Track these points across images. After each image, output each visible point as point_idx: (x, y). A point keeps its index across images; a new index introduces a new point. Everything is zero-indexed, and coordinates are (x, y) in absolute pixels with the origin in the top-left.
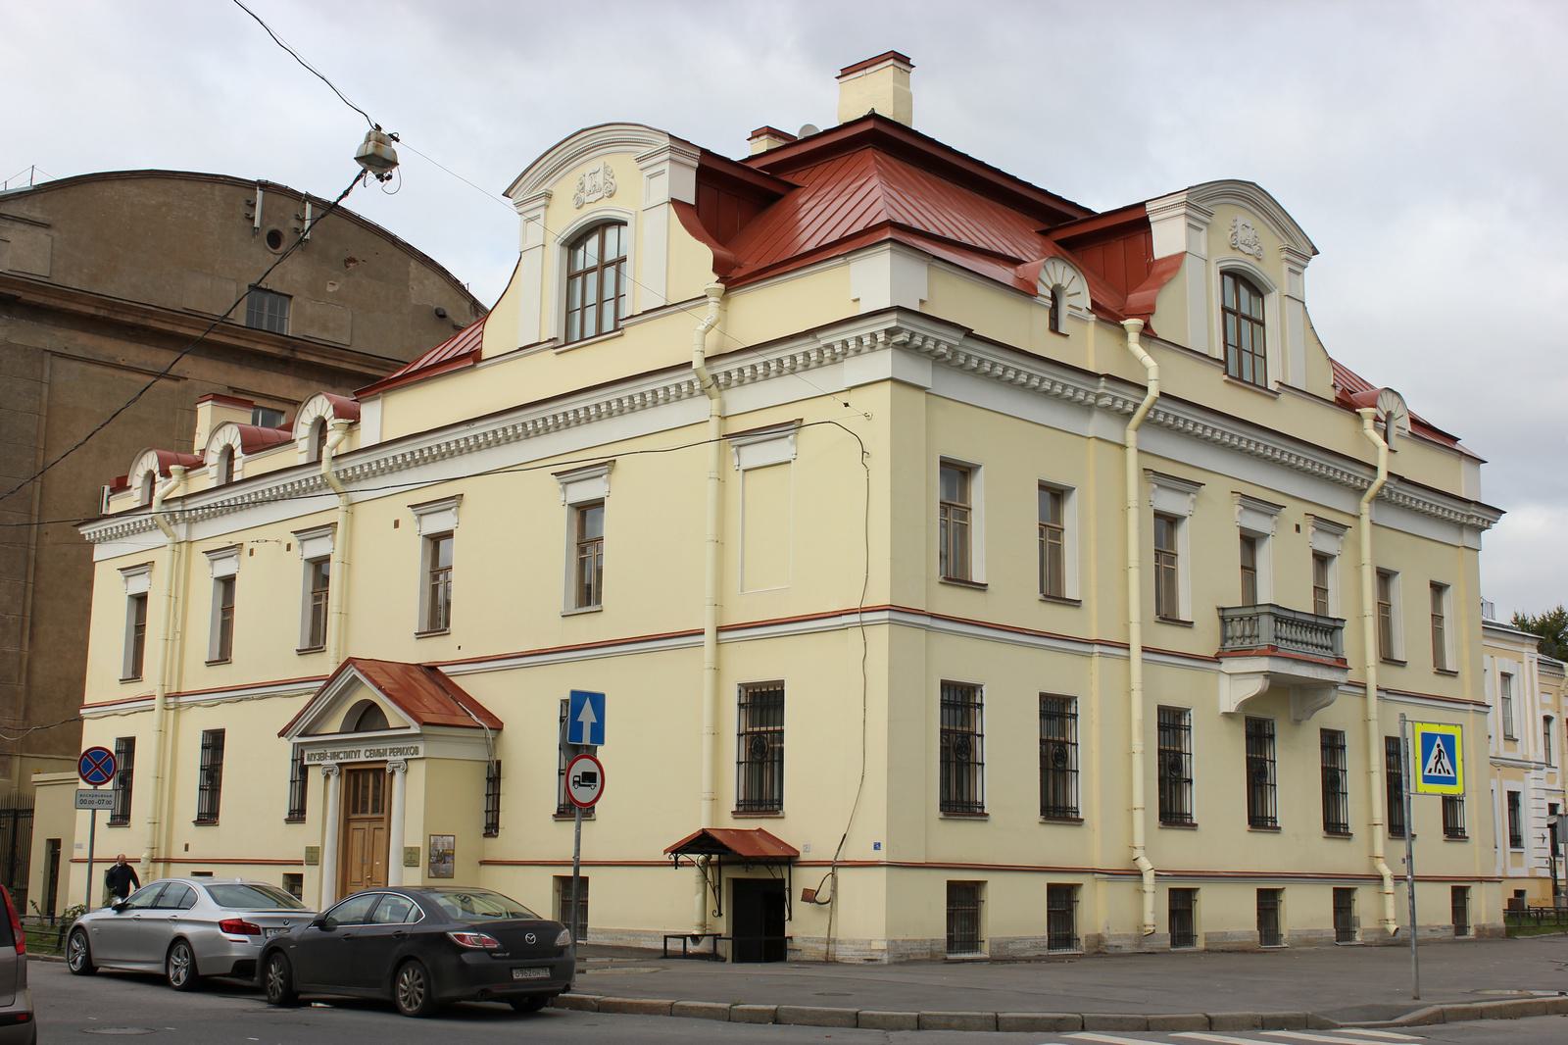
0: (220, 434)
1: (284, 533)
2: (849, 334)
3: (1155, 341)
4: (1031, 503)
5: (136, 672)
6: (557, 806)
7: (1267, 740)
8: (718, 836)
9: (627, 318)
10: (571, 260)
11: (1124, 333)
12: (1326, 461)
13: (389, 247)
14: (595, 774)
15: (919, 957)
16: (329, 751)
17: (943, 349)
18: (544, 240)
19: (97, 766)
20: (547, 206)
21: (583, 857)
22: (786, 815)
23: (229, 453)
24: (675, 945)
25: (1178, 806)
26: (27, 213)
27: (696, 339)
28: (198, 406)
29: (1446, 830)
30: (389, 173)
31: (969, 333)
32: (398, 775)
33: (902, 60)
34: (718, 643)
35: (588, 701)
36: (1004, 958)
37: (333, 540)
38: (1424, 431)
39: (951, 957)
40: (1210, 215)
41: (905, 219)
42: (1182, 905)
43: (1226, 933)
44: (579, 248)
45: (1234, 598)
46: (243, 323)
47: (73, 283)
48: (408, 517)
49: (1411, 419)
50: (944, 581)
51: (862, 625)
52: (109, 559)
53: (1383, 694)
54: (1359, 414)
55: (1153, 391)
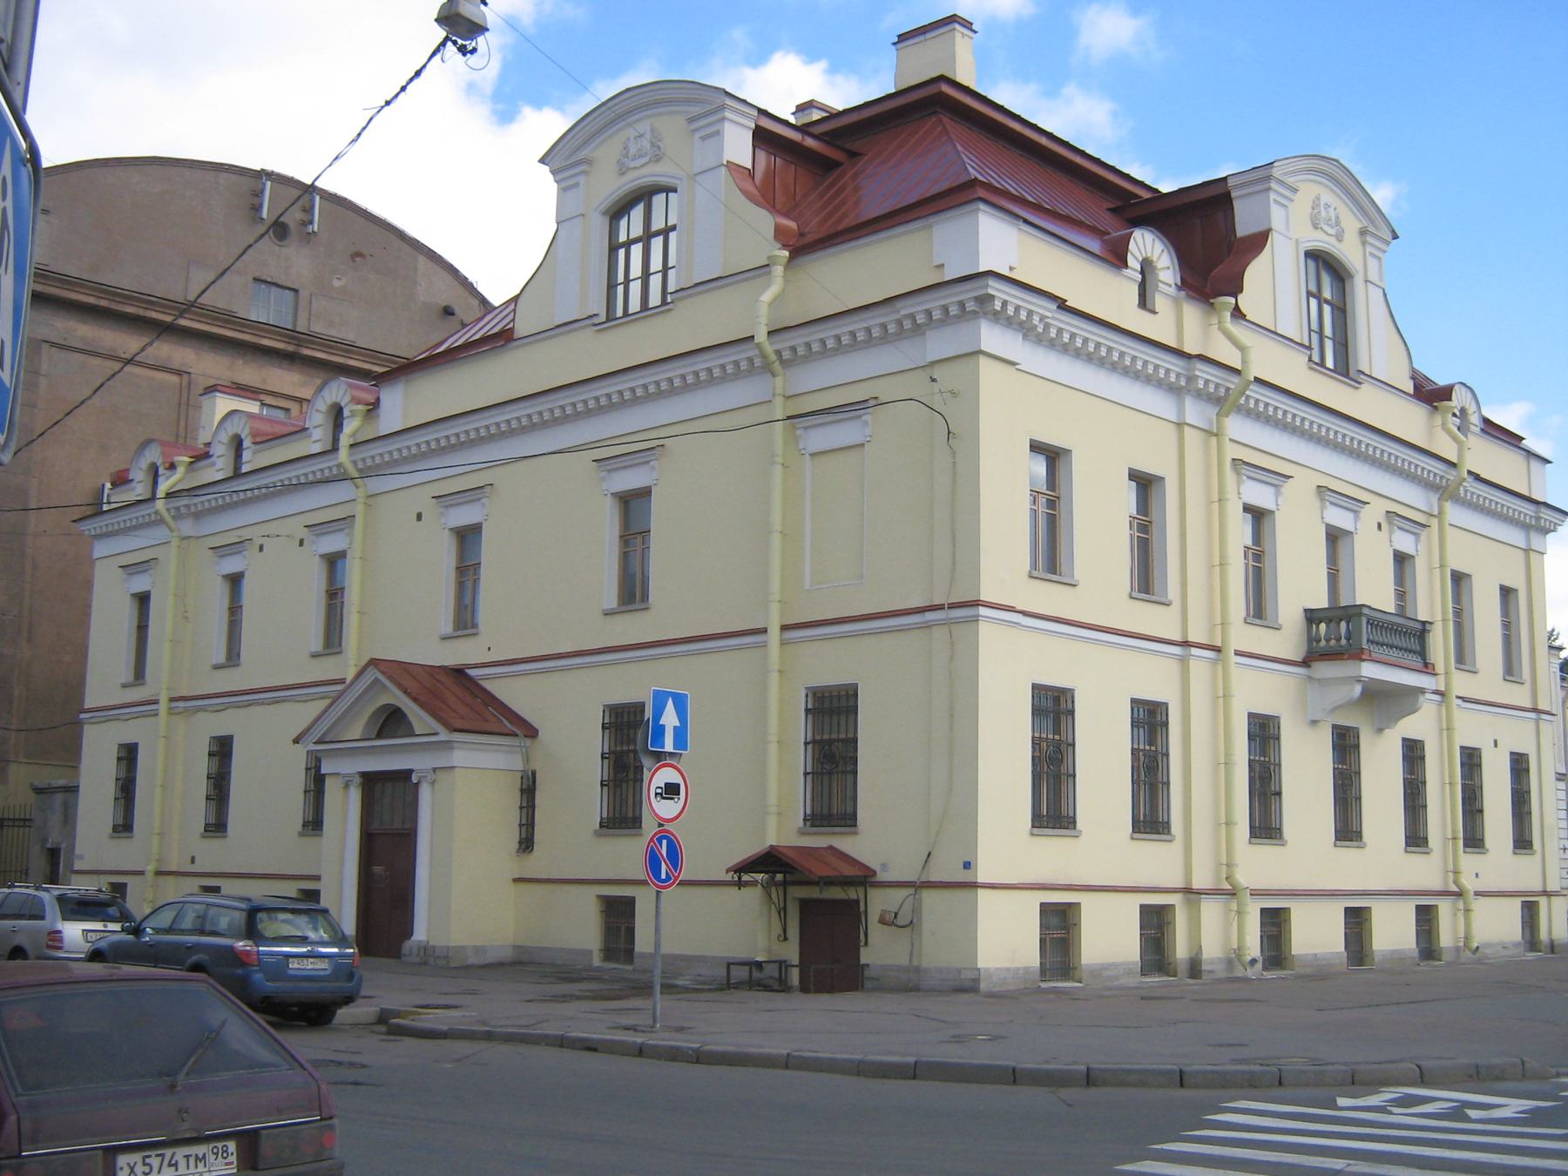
0: (228, 424)
1: (297, 528)
2: (934, 302)
6: (599, 820)
10: (613, 232)
12: (1409, 455)
13: (398, 243)
14: (678, 785)
23: (237, 444)
25: (1165, 815)
30: (474, 44)
31: (1062, 305)
34: (783, 643)
39: (1044, 985)
40: (1295, 190)
44: (623, 216)
45: (1321, 601)
47: (73, 271)
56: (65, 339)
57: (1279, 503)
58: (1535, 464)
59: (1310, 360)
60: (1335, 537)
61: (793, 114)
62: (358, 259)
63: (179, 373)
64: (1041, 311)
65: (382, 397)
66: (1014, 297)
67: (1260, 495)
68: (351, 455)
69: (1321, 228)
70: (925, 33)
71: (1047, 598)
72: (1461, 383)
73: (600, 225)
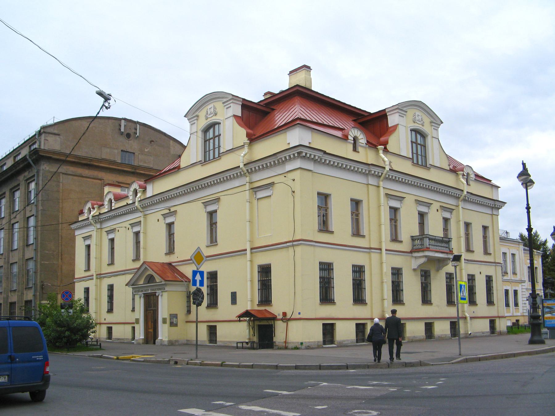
1: (127, 225)
2: (287, 154)
3: (388, 153)
4: (315, 202)
5: (88, 269)
7: (428, 277)
8: (253, 312)
9: (222, 153)
11: (377, 150)
15: (314, 347)
16: (140, 290)
17: (317, 158)
18: (197, 130)
19: (67, 296)
20: (197, 120)
21: (199, 320)
22: (273, 305)
23: (110, 201)
24: (240, 345)
26: (53, 131)
27: (241, 158)
28: (104, 187)
29: (488, 302)
31: (325, 152)
32: (160, 297)
33: (309, 68)
34: (251, 253)
35: (198, 273)
36: (342, 345)
37: (141, 226)
38: (480, 179)
41: (311, 119)
42: (429, 327)
43: (415, 336)
45: (416, 233)
46: (120, 162)
48: (161, 218)
49: (475, 175)
50: (319, 231)
51: (293, 246)
52: (79, 234)
53: (466, 261)
54: (457, 173)
55: (387, 168)
56: (67, 172)
57: (402, 205)
58: (494, 189)
59: (413, 162)
60: (422, 215)
61: (263, 96)
62: (152, 143)
63: (100, 180)
64: (318, 155)
65: (147, 187)
66: (309, 152)
67: (395, 204)
68: (139, 204)
69: (416, 122)
70: (296, 71)
71: (324, 237)
72: (467, 165)
73: (200, 134)
